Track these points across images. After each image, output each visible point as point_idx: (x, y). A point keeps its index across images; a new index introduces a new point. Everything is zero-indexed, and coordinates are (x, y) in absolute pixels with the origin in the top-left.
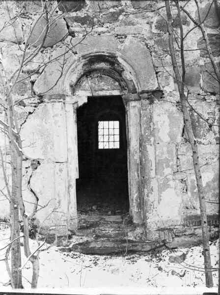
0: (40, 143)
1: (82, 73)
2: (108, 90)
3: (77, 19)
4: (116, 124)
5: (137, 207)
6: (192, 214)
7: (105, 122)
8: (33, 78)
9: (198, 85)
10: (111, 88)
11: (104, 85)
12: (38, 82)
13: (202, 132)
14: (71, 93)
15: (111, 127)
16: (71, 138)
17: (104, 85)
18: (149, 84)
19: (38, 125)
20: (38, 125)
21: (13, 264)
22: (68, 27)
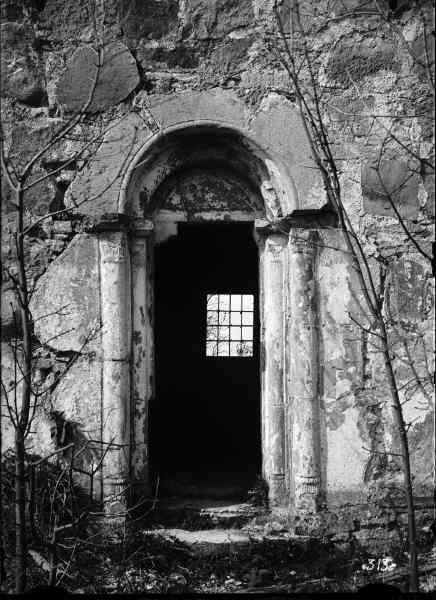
0: (74, 318)
1: (168, 172)
2: (222, 209)
3: (159, 55)
4: (249, 299)
5: (277, 464)
6: (13, 301)
7: (222, 297)
8: (65, 175)
9: (413, 202)
10: (229, 206)
11: (214, 199)
12: (74, 186)
13: (420, 303)
14: (142, 212)
15: (236, 306)
16: (141, 309)
17: (214, 199)
18: (310, 196)
19: (72, 280)
20: (72, 280)
21: (324, 452)
22: (141, 71)
